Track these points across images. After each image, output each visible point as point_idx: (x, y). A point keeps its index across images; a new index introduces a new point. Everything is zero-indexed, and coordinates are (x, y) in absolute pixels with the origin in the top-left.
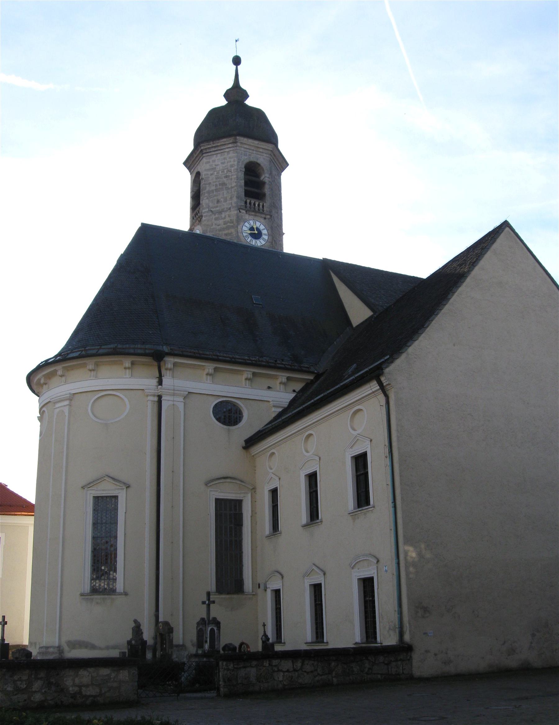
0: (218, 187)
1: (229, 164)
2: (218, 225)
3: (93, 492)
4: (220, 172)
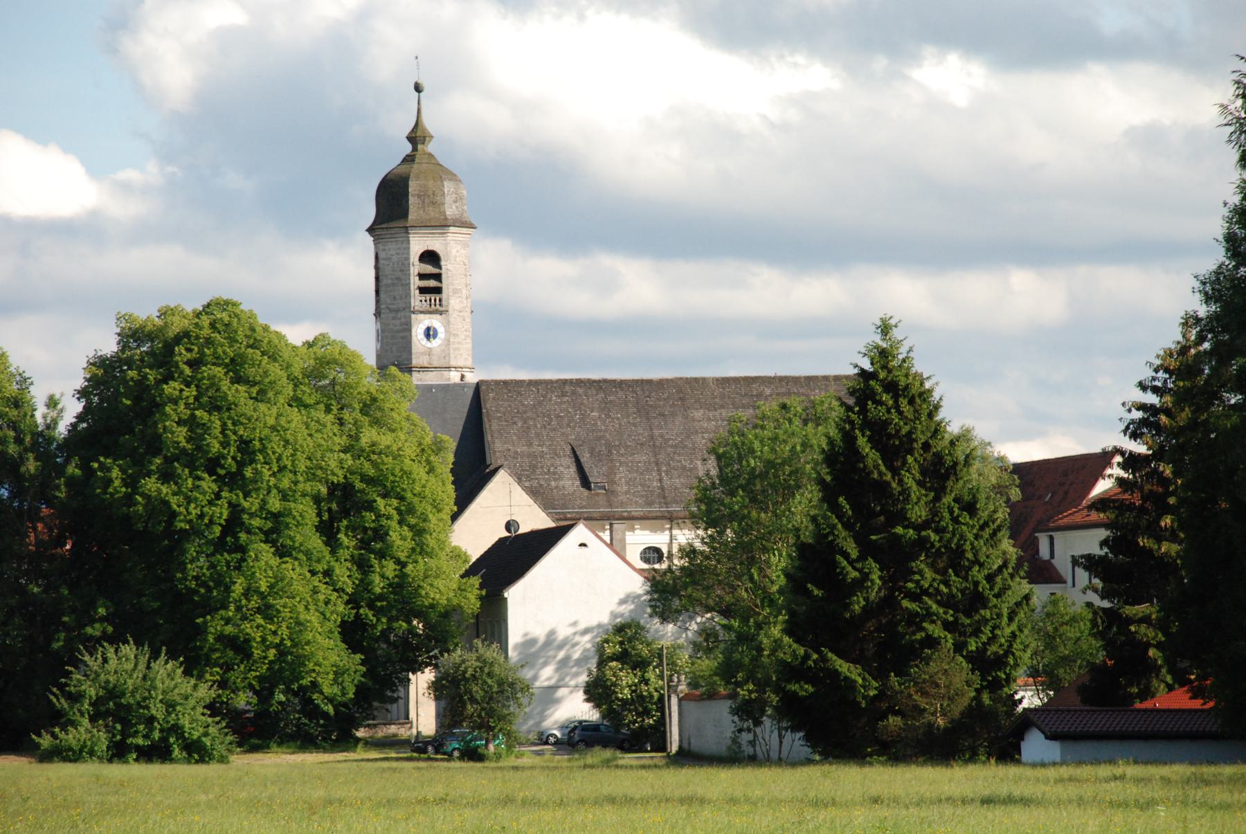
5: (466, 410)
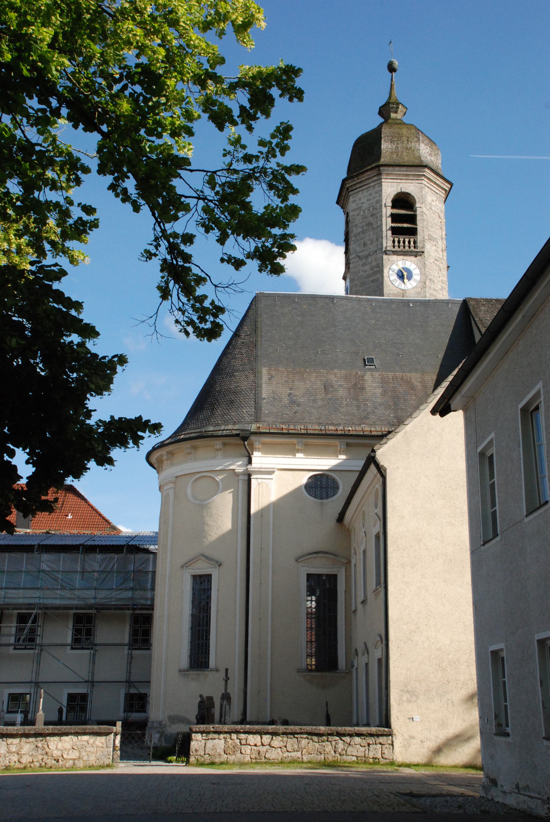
0: (365, 228)
1: (375, 200)
2: (365, 272)
3: (191, 571)
4: (366, 210)
5: (452, 324)
